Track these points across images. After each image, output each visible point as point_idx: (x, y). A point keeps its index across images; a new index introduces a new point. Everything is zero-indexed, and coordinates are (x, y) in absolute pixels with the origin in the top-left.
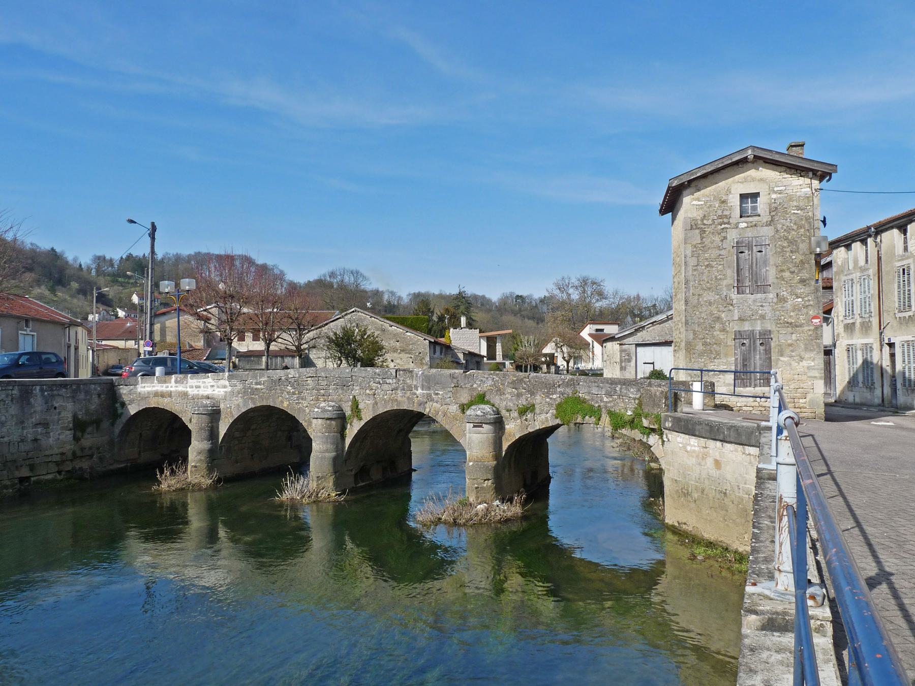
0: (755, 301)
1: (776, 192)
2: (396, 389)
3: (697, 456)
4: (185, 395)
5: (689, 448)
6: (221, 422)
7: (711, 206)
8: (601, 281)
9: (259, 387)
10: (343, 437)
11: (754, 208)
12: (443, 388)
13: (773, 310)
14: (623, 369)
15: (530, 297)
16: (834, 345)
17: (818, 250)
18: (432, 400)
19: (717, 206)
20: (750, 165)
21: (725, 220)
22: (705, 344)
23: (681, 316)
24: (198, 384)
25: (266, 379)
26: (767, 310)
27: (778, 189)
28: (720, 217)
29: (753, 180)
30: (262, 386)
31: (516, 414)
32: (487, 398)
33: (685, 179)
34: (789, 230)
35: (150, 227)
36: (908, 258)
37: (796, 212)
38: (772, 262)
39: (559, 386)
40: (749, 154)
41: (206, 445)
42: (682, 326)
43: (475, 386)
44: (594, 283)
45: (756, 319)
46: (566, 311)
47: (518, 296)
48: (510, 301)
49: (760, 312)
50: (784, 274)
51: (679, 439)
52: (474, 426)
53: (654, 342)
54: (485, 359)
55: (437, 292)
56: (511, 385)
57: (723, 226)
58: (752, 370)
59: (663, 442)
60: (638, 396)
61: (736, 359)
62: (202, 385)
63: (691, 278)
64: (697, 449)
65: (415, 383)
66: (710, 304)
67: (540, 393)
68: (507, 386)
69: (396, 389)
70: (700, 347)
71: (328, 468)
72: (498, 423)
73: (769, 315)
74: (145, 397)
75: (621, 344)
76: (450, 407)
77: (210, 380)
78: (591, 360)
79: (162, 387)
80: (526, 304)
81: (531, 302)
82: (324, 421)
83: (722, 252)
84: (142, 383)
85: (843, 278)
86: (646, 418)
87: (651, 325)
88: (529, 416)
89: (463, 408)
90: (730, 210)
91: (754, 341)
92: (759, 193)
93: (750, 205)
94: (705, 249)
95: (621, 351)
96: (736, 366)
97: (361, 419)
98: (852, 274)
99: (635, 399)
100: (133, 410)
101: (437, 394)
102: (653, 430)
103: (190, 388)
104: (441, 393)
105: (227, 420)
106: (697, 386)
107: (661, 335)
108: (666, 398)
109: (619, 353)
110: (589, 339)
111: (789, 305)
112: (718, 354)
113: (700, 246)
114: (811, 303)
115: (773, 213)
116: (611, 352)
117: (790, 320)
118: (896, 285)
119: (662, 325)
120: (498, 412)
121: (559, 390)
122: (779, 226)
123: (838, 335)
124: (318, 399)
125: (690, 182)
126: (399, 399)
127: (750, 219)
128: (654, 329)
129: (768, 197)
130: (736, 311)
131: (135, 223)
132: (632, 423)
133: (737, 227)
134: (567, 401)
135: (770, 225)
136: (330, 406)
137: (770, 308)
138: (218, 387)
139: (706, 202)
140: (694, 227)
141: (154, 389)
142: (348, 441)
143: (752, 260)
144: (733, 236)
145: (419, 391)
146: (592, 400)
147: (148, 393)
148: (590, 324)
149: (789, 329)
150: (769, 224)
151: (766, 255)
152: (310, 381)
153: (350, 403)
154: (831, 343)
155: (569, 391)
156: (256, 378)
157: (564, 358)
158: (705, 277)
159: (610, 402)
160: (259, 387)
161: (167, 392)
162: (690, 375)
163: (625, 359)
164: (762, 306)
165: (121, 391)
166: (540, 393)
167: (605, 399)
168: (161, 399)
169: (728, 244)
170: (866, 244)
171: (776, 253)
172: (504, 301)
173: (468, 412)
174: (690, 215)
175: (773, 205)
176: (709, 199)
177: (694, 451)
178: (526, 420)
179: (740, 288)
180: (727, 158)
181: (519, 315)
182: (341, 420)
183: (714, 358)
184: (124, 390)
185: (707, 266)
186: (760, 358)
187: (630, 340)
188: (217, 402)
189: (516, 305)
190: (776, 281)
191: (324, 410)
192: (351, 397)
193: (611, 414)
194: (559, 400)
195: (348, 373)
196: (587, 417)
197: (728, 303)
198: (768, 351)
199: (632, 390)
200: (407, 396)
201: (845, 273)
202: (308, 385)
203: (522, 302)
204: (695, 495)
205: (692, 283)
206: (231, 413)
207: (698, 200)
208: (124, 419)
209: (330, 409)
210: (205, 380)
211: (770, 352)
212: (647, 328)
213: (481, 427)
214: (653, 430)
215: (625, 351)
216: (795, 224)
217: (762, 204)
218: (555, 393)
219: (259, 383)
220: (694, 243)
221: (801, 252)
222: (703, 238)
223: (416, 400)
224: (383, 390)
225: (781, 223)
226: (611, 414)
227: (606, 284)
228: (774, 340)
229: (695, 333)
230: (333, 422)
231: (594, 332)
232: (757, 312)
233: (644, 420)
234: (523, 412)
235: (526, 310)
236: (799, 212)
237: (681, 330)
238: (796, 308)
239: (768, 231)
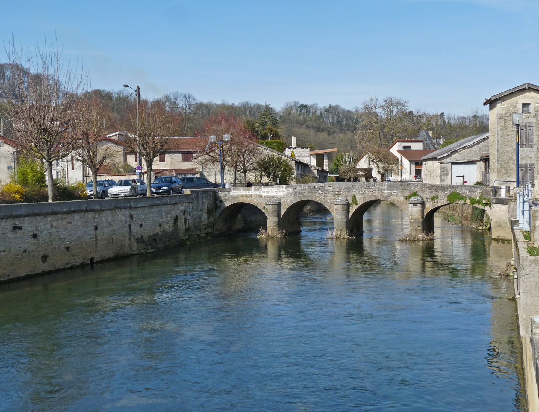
0: (527, 151)
2: (375, 191)
3: (505, 211)
4: (260, 196)
5: (501, 209)
6: (282, 208)
7: (509, 108)
8: (406, 102)
9: (303, 191)
10: (348, 213)
11: (528, 110)
12: (397, 190)
14: (442, 180)
15: (314, 106)
18: (392, 195)
20: (527, 91)
22: (506, 170)
23: (495, 157)
24: (268, 191)
25: (307, 187)
26: (533, 155)
29: (528, 97)
30: (305, 191)
31: (430, 200)
32: (418, 193)
33: (498, 97)
35: (136, 88)
38: (535, 133)
39: (449, 188)
40: (526, 86)
41: (276, 219)
42: (495, 161)
43: (412, 189)
44: (398, 103)
45: (528, 159)
46: (373, 129)
47: (302, 106)
48: (294, 111)
49: (530, 156)
51: (498, 206)
52: (414, 205)
53: (464, 161)
54: (329, 174)
55: (219, 102)
56: (428, 188)
58: (526, 181)
59: (491, 208)
60: (481, 192)
62: (270, 191)
63: (500, 141)
64: (504, 209)
65: (384, 188)
66: (508, 152)
67: (441, 191)
68: (427, 189)
69: (375, 191)
70: (503, 171)
71: (343, 225)
72: (423, 204)
73: (534, 157)
74: (234, 198)
75: (441, 163)
77: (275, 188)
78: (400, 174)
79: (246, 192)
80: (311, 114)
81: (316, 112)
82: (342, 206)
84: (233, 191)
86: (484, 200)
87: (462, 149)
88: (436, 200)
89: (407, 198)
91: (527, 168)
92: (530, 103)
93: (526, 108)
95: (441, 168)
97: (357, 204)
99: (480, 193)
100: (227, 204)
102: (487, 204)
103: (263, 192)
104: (396, 192)
105: (285, 207)
106: (503, 187)
107: (469, 157)
108: (493, 192)
109: (439, 170)
110: (398, 155)
113: (504, 126)
115: (536, 112)
116: (432, 169)
119: (469, 149)
120: (423, 200)
121: (448, 190)
124: (335, 196)
125: (500, 98)
126: (376, 195)
127: (526, 115)
128: (464, 152)
129: (534, 105)
131: (128, 87)
132: (479, 202)
134: (452, 194)
135: (535, 117)
136: (344, 199)
137: (534, 154)
138: (279, 192)
139: (507, 107)
141: (241, 193)
142: (351, 214)
143: (527, 133)
145: (386, 192)
146: (463, 193)
147: (237, 195)
148: (399, 141)
150: (534, 117)
151: (532, 131)
152: (330, 188)
153: (352, 198)
155: (453, 190)
156: (302, 187)
157: (379, 172)
158: (506, 140)
160: (303, 191)
161: (249, 195)
162: (499, 183)
163: (444, 174)
164: (530, 153)
165: (220, 195)
166: (441, 191)
168: (245, 199)
171: (537, 130)
172: (288, 110)
173: (411, 200)
174: (500, 112)
177: (503, 210)
178: (435, 202)
179: (521, 145)
180: (516, 88)
181: (304, 125)
182: (348, 205)
183: (510, 176)
184: (222, 195)
185: (507, 135)
186: (529, 176)
188: (279, 199)
189: (300, 115)
190: (536, 142)
191: (341, 201)
192: (352, 195)
193: (470, 199)
194: (449, 194)
195: (351, 184)
196: (460, 200)
198: (533, 173)
199: (479, 189)
202: (329, 190)
203: (307, 112)
204: (504, 225)
205: (500, 143)
206: (287, 204)
207: (503, 105)
208: (222, 209)
209: (344, 200)
210: (272, 189)
212: (459, 151)
213: (417, 205)
214: (487, 204)
215: (444, 168)
217: (531, 108)
218: (447, 191)
219: (303, 190)
220: (502, 125)
222: (506, 122)
223: (384, 195)
226: (470, 199)
227: (409, 104)
228: (535, 168)
229: (501, 164)
230: (345, 206)
231: (402, 149)
233: (483, 201)
234: (433, 199)
235: (311, 120)
237: (495, 163)
239: (533, 120)
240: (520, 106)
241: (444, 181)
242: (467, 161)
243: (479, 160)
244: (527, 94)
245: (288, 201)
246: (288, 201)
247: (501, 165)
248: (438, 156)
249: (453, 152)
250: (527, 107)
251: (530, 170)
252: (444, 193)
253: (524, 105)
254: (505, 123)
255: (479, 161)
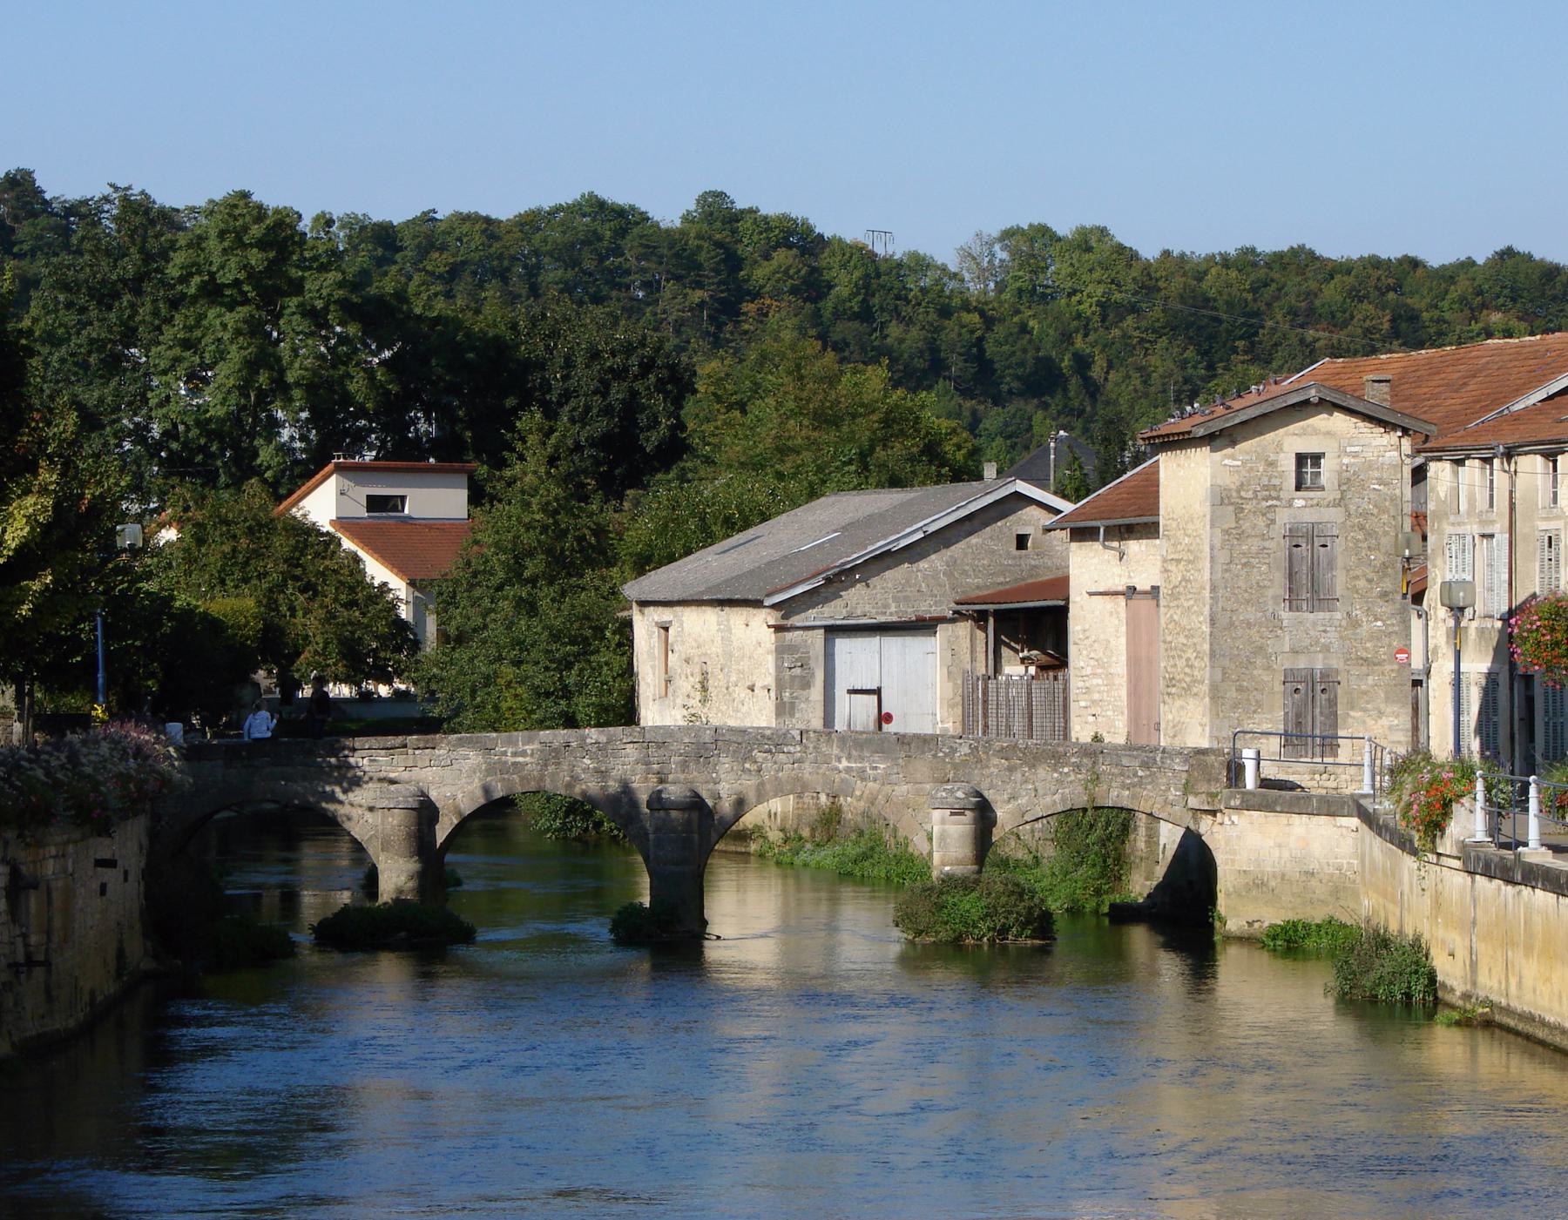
1: (1348, 455)
9: (520, 759)
13: (1341, 637)
16: (1428, 673)
17: (1407, 553)
19: (1261, 469)
21: (1274, 494)
22: (1240, 689)
27: (1353, 449)
28: (1266, 488)
29: (1316, 432)
30: (528, 759)
34: (1366, 514)
36: (1557, 518)
37: (1376, 487)
38: (1340, 562)
45: (1316, 652)
50: (1357, 582)
52: (952, 814)
53: (882, 619)
57: (1270, 503)
61: (1286, 714)
66: (1249, 625)
70: (1232, 694)
76: (896, 788)
83: (1267, 544)
85: (1449, 529)
90: (1281, 477)
94: (1241, 536)
96: (1286, 724)
98: (1464, 524)
101: (876, 768)
111: (1363, 631)
112: (1259, 704)
114: (1396, 628)
115: (1344, 487)
117: (1364, 655)
118: (1537, 568)
122: (1352, 508)
123: (1436, 648)
127: (1311, 494)
130: (1287, 638)
133: (1291, 506)
140: (1226, 501)
144: (1283, 517)
149: (1364, 668)
150: (1338, 503)
154: (1421, 667)
158: (1240, 583)
159: (1146, 777)
160: (520, 759)
163: (793, 678)
164: (1324, 631)
167: (1140, 773)
169: (1279, 529)
170: (1491, 465)
174: (1219, 482)
175: (1345, 474)
176: (1248, 457)
183: (1255, 712)
186: (1321, 713)
187: (813, 616)
197: (1275, 623)
198: (1333, 703)
200: (821, 771)
201: (1452, 518)
211: (1336, 704)
213: (963, 814)
216: (1375, 506)
218: (1067, 765)
219: (524, 754)
220: (1226, 527)
221: (1383, 550)
224: (775, 763)
225: (1355, 503)
232: (1317, 642)
236: (1381, 487)
238: (1375, 636)
239: (1334, 515)
240: (1289, 465)
241: (792, 715)
242: (895, 619)
243: (950, 614)
244: (1320, 421)
245: (460, 796)
246: (460, 796)
247: (1224, 674)
248: (768, 595)
249: (835, 575)
250: (1313, 466)
251: (1323, 691)
252: (1056, 771)
253: (1301, 459)
254: (1238, 520)
255: (952, 621)
